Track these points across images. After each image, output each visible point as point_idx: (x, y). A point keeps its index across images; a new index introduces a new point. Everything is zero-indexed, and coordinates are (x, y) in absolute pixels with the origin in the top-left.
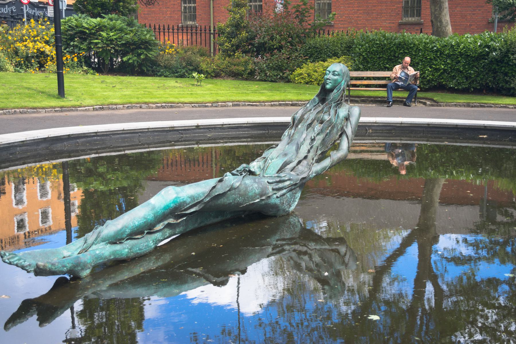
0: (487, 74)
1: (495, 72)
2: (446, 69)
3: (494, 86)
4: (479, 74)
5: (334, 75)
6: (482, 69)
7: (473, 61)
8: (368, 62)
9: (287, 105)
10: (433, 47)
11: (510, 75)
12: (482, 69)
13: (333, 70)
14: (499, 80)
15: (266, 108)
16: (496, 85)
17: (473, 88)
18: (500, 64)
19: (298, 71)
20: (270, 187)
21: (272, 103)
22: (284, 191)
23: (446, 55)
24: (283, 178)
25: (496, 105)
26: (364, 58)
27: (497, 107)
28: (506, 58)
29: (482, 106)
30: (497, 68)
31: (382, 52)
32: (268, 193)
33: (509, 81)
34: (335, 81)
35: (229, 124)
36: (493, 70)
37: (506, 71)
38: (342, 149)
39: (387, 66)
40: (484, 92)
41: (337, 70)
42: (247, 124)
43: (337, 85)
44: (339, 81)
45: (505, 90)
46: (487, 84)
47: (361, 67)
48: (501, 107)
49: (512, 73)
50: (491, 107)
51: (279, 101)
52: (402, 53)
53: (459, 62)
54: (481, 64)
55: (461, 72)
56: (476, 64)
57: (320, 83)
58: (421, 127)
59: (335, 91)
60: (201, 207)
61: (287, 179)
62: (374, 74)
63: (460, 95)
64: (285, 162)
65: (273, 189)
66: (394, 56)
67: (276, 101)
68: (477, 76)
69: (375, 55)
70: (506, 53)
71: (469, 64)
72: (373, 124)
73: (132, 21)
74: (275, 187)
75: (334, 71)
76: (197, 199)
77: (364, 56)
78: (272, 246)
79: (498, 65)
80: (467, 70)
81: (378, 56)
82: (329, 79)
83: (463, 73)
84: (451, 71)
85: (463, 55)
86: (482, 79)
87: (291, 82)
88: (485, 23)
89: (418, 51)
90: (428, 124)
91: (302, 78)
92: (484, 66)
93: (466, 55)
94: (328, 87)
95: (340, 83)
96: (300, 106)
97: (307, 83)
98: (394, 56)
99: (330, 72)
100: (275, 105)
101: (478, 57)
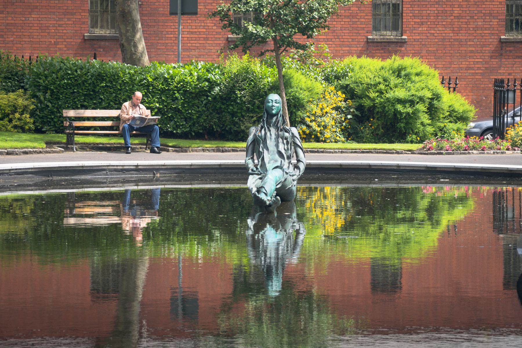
0: (211, 114)
1: (219, 111)
2: (161, 108)
3: (219, 130)
4: (201, 115)
6: (204, 108)
7: (192, 98)
10: (141, 80)
11: (239, 115)
12: (204, 108)
14: (225, 121)
18: (225, 102)
23: (159, 90)
26: (52, 92)
30: (223, 107)
31: (77, 85)
33: (237, 123)
34: (278, 107)
35: (16, 169)
37: (235, 110)
39: (85, 103)
42: (32, 168)
46: (211, 126)
49: (241, 112)
52: (103, 87)
53: (176, 98)
54: (202, 102)
56: (196, 101)
58: (212, 169)
68: (198, 117)
71: (188, 103)
72: (161, 167)
73: (400, 77)
75: (276, 100)
77: (52, 90)
79: (223, 104)
84: (167, 111)
85: (180, 90)
86: (205, 121)
88: (80, 41)
90: (220, 165)
92: (206, 105)
93: (183, 90)
94: (274, 112)
96: (17, 154)
98: (93, 91)
99: (272, 101)
101: (197, 94)
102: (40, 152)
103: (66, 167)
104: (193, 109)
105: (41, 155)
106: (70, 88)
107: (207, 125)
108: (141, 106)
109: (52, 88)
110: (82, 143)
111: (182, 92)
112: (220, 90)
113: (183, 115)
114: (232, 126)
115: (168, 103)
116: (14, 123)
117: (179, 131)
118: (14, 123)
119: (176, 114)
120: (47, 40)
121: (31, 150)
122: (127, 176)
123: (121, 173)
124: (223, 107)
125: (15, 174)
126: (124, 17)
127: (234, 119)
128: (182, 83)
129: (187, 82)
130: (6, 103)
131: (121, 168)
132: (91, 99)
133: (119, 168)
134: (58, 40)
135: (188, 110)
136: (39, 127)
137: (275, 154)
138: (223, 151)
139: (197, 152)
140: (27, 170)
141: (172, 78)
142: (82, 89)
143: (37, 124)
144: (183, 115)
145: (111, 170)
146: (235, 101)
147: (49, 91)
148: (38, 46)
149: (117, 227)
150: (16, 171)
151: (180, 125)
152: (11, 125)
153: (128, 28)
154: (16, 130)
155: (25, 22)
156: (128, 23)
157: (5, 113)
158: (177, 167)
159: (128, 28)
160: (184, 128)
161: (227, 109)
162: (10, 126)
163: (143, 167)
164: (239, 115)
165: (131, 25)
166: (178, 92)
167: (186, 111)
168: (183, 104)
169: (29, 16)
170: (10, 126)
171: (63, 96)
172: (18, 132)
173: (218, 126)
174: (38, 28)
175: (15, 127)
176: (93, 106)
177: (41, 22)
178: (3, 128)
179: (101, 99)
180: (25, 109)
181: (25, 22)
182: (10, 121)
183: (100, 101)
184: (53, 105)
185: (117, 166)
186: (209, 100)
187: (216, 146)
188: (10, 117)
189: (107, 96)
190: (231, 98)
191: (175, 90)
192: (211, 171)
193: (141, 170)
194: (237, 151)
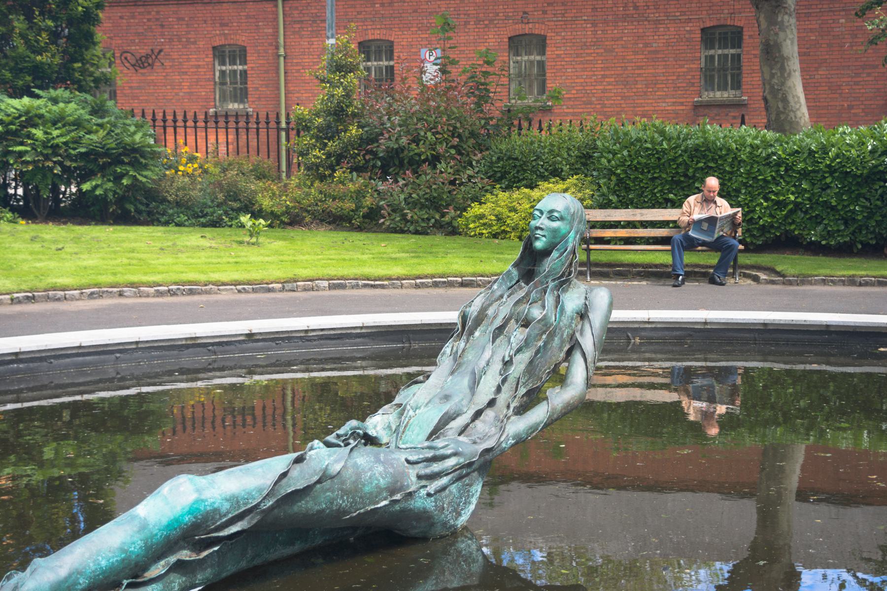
2: (801, 203)
6: (879, 203)
7: (858, 184)
8: (628, 189)
9: (451, 284)
12: (879, 203)
13: (550, 208)
19: (476, 209)
20: (412, 473)
21: (418, 281)
22: (445, 480)
23: (799, 172)
24: (442, 452)
26: (620, 181)
31: (658, 166)
32: (408, 486)
34: (555, 231)
39: (671, 196)
42: (361, 328)
52: (702, 169)
53: (828, 186)
54: (876, 190)
55: (833, 208)
56: (864, 191)
59: (555, 254)
60: (254, 522)
61: (449, 452)
62: (642, 215)
64: (446, 414)
65: (420, 477)
66: (686, 176)
67: (426, 277)
68: (868, 218)
69: (642, 173)
71: (850, 192)
72: (642, 326)
74: (422, 472)
75: (551, 211)
76: (245, 504)
80: (845, 203)
81: (650, 176)
82: (542, 229)
83: (838, 211)
84: (811, 208)
85: (835, 171)
89: (736, 163)
91: (484, 224)
92: (882, 196)
93: (841, 173)
94: (539, 245)
97: (495, 236)
98: (686, 176)
99: (542, 212)
101: (868, 177)
103: (441, 324)
106: (649, 172)
109: (619, 171)
111: (837, 174)
119: (828, 213)
120: (838, 104)
125: (318, 340)
126: (768, 53)
129: (848, 158)
134: (853, 103)
135: (848, 205)
139: (811, 284)
141: (824, 150)
142: (667, 173)
148: (826, 111)
149: (676, 406)
150: (321, 333)
153: (774, 71)
155: (810, 81)
156: (773, 63)
158: (677, 326)
159: (774, 71)
160: (842, 236)
165: (779, 66)
167: (845, 207)
168: (839, 195)
169: (815, 73)
174: (827, 88)
177: (831, 80)
181: (810, 81)
192: (747, 335)
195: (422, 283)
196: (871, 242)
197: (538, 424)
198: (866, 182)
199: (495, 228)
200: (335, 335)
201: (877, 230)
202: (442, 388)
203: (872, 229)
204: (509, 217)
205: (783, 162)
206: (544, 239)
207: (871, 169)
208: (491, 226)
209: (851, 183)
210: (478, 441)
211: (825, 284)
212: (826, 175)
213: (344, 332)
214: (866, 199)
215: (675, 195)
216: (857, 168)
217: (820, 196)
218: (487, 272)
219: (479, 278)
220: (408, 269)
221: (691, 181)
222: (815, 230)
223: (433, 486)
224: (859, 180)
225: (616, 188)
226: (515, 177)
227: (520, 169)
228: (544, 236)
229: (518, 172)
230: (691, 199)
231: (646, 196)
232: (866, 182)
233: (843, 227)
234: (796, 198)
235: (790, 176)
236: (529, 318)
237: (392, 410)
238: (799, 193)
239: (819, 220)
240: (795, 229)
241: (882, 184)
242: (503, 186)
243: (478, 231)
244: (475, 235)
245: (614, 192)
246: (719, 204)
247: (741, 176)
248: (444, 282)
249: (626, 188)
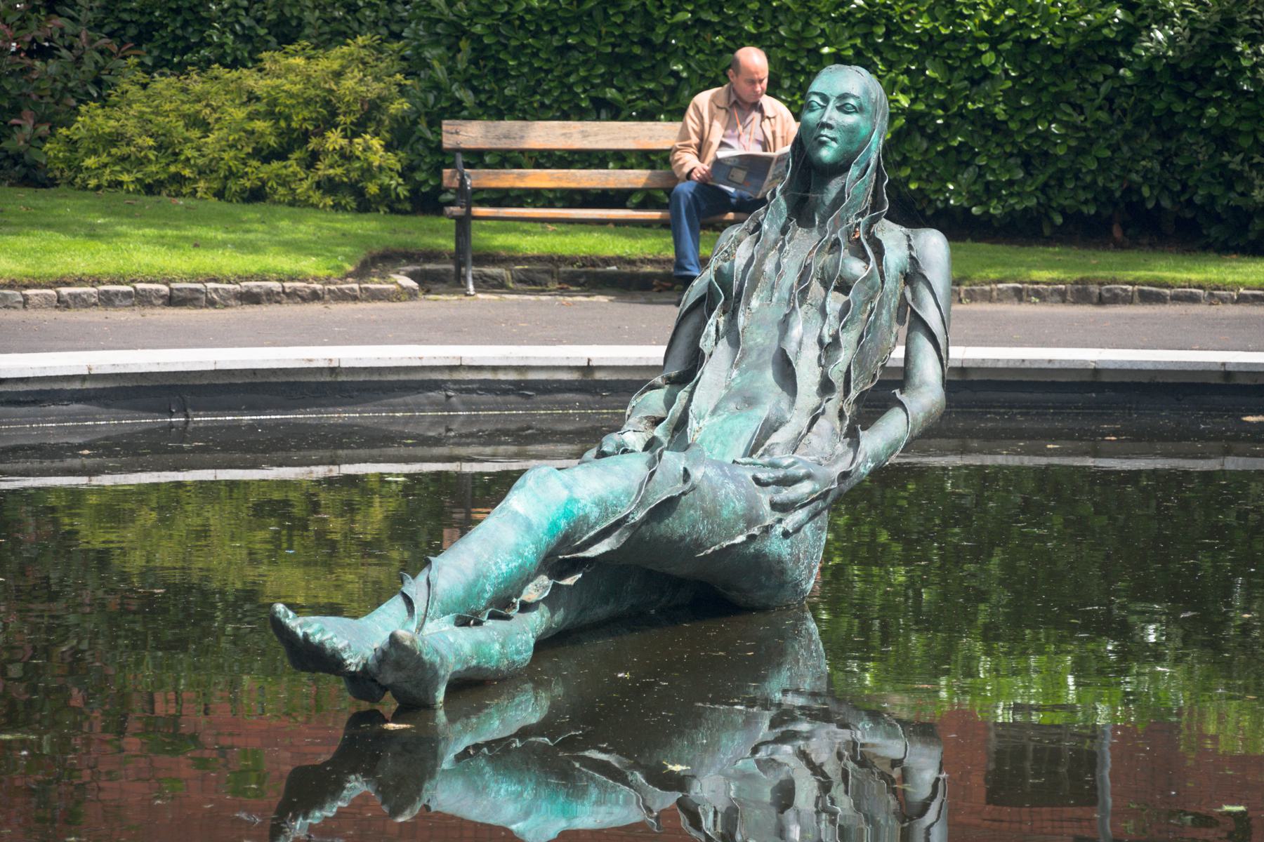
0: (1128, 137)
1: (1166, 128)
2: (922, 115)
3: (1166, 203)
5: (842, 109)
6: (1103, 116)
7: (1055, 69)
8: (501, 74)
9: (143, 299)
11: (1245, 142)
12: (1103, 116)
13: (839, 90)
14: (1189, 167)
15: (31, 315)
16: (1174, 196)
17: (1063, 212)
18: (1190, 86)
19: (92, 120)
20: (765, 497)
21: (65, 291)
22: (801, 515)
23: (917, 40)
24: (791, 471)
25: (1214, 294)
26: (480, 52)
27: (1223, 300)
28: (1224, 60)
29: (1147, 298)
30: (1179, 107)
31: (577, 19)
32: (764, 519)
33: (1239, 175)
34: (851, 131)
36: (1158, 121)
37: (1228, 122)
38: (923, 383)
39: (611, 93)
40: (1117, 232)
41: (855, 93)
42: (83, 378)
43: (855, 147)
44: (864, 132)
45: (1218, 219)
46: (1131, 189)
47: (467, 97)
48: (1242, 299)
50: (1193, 299)
51: (96, 280)
52: (684, 26)
53: (986, 74)
54: (1096, 85)
55: (998, 127)
56: (1071, 86)
57: (233, 186)
59: (854, 171)
60: (623, 540)
61: (802, 472)
62: (585, 135)
63: (1013, 249)
64: (767, 420)
65: (774, 506)
66: (645, 42)
67: (80, 281)
68: (1078, 152)
69: (535, 35)
70: (1221, 32)
71: (1037, 90)
74: (777, 498)
75: (843, 96)
76: (614, 513)
77: (479, 38)
78: (774, 712)
79: (1183, 96)
80: (1028, 116)
81: (556, 42)
82: (830, 127)
83: (1009, 134)
84: (947, 125)
85: (1003, 38)
86: (1104, 165)
87: (50, 183)
89: (767, 14)
91: (123, 159)
92: (1109, 99)
93: (1016, 41)
94: (827, 154)
95: (866, 140)
96: (212, 303)
97: (151, 189)
98: (645, 42)
99: (825, 99)
100: (80, 302)
101: (1078, 53)
102: (315, 296)
103: (254, 372)
104: (1055, 120)
105: (315, 308)
106: (554, 31)
107: (1115, 185)
108: (768, 102)
109: (478, 29)
110: (539, 259)
111: (1007, 46)
112: (1171, 40)
113: (1014, 144)
114: (1217, 191)
115: (951, 94)
116: (324, 169)
117: (995, 209)
118: (324, 169)
119: (987, 140)
121: (275, 286)
122: (542, 413)
123: (512, 398)
124: (1179, 107)
127: (1226, 158)
128: (1009, 12)
130: (295, 89)
131: (512, 376)
132: (638, 76)
133: (502, 376)
135: (1035, 121)
136: (424, 189)
137: (759, 367)
138: (1101, 301)
140: (57, 386)
142: (599, 37)
143: (420, 176)
144: (1014, 144)
145: (465, 388)
146: (1230, 84)
147: (464, 44)
151: (999, 185)
152: (313, 177)
154: (329, 201)
157: (290, 129)
160: (1019, 194)
161: (1199, 118)
162: (305, 184)
163: (614, 377)
164: (1245, 142)
166: (993, 48)
167: (1026, 124)
168: (1011, 97)
170: (305, 184)
171: (521, 64)
172: (337, 207)
173: (1165, 188)
175: (329, 186)
176: (642, 104)
178: (281, 190)
179: (675, 74)
180: (368, 117)
182: (312, 160)
183: (672, 82)
184: (483, 97)
185: (495, 369)
186: (1123, 78)
187: (1077, 275)
188: (311, 146)
189: (699, 62)
190: (1213, 70)
191: (982, 40)
193: (605, 385)
194: (1158, 299)
195: (75, 297)
196: (1085, 209)
197: (898, 441)
198: (1073, 65)
199: (153, 168)
200: (27, 393)
201: (1100, 181)
202: (727, 387)
203: (1088, 179)
204: (187, 140)
205: (881, 15)
206: (834, 144)
207: (1085, 34)
208: (142, 162)
209: (1038, 67)
210: (824, 462)
211: (1021, 300)
212: (983, 47)
213: (46, 387)
214: (1074, 106)
215: (620, 90)
216: (1052, 32)
217: (967, 98)
218: (226, 271)
219: (211, 285)
220: (28, 261)
221: (659, 56)
222: (954, 181)
223: (792, 520)
224: (1059, 59)
225: (473, 70)
226: (176, 38)
227: (189, 16)
228: (834, 139)
229: (186, 24)
230: (704, 99)
231: (547, 93)
232: (1073, 65)
233: (1020, 174)
234: (913, 101)
235: (894, 47)
236: (847, 275)
237: (641, 427)
238: (918, 91)
239: (965, 158)
240: (909, 179)
241: (1110, 70)
242: (148, 61)
243: (107, 176)
244: (98, 187)
245: (467, 83)
246: (768, 112)
247: (780, 46)
248: (127, 295)
249: (494, 71)
